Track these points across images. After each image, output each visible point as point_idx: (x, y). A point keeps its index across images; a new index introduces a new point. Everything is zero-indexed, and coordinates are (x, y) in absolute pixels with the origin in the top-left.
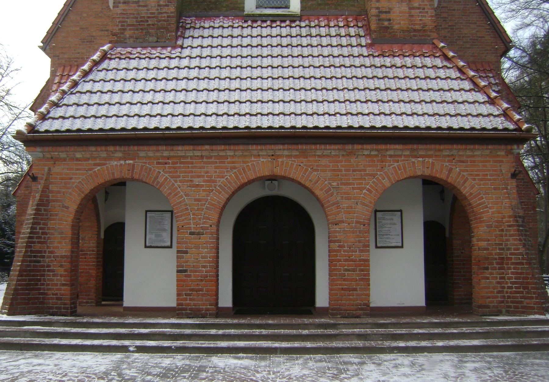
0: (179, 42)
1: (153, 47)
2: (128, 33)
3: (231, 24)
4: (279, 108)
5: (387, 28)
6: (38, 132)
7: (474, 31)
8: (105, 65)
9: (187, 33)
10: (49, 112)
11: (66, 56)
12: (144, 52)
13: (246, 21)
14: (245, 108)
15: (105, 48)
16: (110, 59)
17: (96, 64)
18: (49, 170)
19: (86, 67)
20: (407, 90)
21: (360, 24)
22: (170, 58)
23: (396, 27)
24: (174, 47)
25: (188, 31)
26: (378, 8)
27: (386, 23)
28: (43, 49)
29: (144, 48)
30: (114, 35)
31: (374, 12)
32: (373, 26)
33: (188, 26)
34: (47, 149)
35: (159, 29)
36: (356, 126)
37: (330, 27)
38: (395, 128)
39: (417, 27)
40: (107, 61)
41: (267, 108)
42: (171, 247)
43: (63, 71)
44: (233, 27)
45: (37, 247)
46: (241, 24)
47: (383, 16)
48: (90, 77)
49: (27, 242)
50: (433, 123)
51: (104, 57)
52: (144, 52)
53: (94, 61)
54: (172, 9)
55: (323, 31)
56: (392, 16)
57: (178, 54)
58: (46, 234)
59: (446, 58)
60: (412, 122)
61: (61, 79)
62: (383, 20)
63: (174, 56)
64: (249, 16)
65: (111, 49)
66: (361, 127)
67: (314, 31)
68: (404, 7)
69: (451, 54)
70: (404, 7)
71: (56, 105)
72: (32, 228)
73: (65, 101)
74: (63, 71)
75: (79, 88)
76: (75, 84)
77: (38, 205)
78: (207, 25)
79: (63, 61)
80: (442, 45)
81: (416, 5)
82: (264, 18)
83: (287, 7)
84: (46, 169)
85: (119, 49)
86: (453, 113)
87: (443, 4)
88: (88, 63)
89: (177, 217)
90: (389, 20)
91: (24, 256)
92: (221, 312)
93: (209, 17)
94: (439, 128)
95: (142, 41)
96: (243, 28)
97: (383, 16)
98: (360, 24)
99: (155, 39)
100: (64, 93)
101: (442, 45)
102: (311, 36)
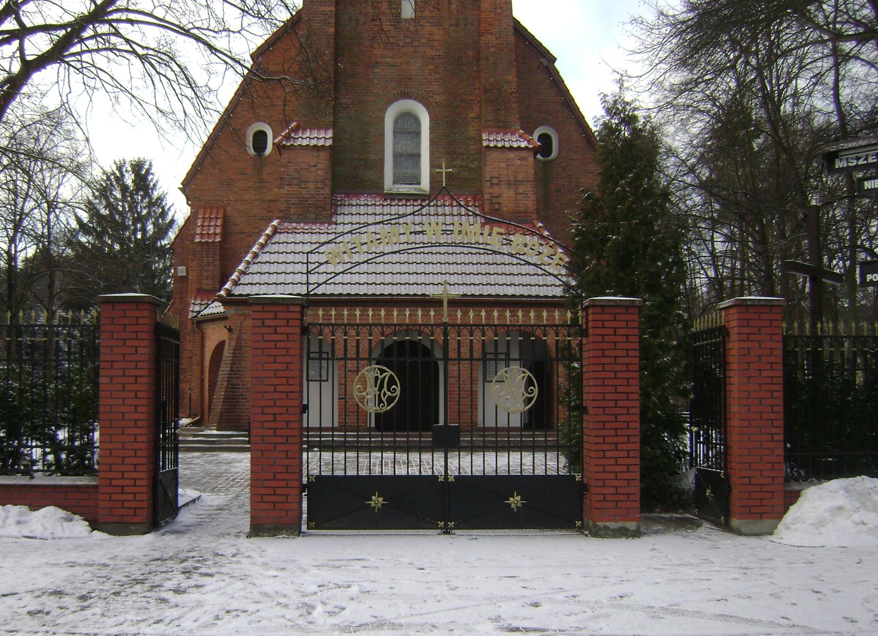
0: (334, 219)
1: (313, 223)
2: (292, 211)
3: (373, 202)
4: (413, 279)
5: (498, 210)
6: (234, 295)
7: (591, 181)
8: (276, 238)
9: (340, 210)
10: (239, 279)
11: (205, 198)
12: (306, 227)
13: (386, 200)
14: (388, 279)
15: (275, 223)
16: (280, 233)
17: (269, 237)
18: (242, 323)
19: (262, 240)
20: (509, 264)
21: (477, 204)
22: (328, 233)
23: (505, 209)
24: (330, 224)
25: (339, 208)
26: (491, 194)
27: (497, 206)
28: (182, 190)
29: (306, 223)
30: (281, 211)
31: (487, 196)
32: (487, 209)
33: (339, 203)
34: (240, 308)
35: (318, 207)
36: (469, 294)
37: (453, 206)
38: (498, 295)
39: (521, 209)
40: (277, 235)
41: (404, 279)
42: (327, 381)
43: (204, 214)
44: (375, 205)
45: (234, 381)
46: (381, 202)
47: (494, 200)
48: (266, 250)
49: (228, 378)
50: (525, 291)
51: (275, 231)
52: (306, 227)
53: (268, 235)
54: (327, 191)
55: (447, 210)
56: (501, 200)
57: (334, 230)
58: (239, 371)
59: (542, 237)
60: (510, 291)
61: (203, 221)
62: (495, 203)
63: (330, 231)
64: (387, 194)
65: (279, 224)
66: (473, 295)
67: (440, 210)
68: (512, 193)
69: (546, 233)
70: (512, 193)
71: (243, 273)
72: (231, 367)
73: (251, 270)
74: (204, 214)
75: (259, 259)
76: (256, 255)
77: (234, 350)
78: (354, 203)
79: (203, 203)
80: (540, 225)
81: (521, 191)
82: (400, 197)
83: (419, 184)
84: (239, 322)
85: (286, 224)
86: (541, 283)
87: (563, 154)
88: (263, 237)
89: (450, 391)
90: (499, 203)
91: (226, 388)
92: (370, 429)
93: (357, 195)
94: (530, 296)
95: (303, 218)
96: (383, 206)
97: (494, 200)
98: (477, 204)
99: (314, 216)
100: (248, 263)
101: (540, 225)
102: (438, 215)
